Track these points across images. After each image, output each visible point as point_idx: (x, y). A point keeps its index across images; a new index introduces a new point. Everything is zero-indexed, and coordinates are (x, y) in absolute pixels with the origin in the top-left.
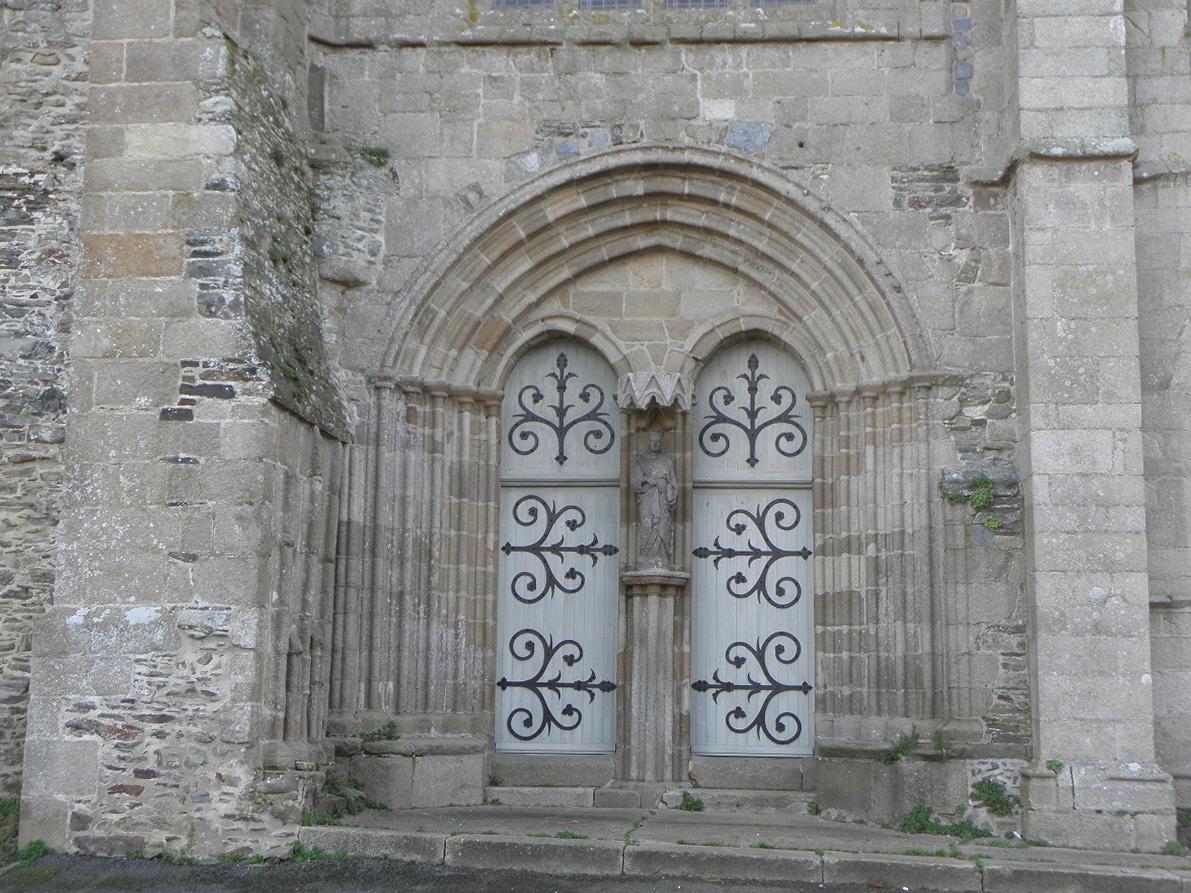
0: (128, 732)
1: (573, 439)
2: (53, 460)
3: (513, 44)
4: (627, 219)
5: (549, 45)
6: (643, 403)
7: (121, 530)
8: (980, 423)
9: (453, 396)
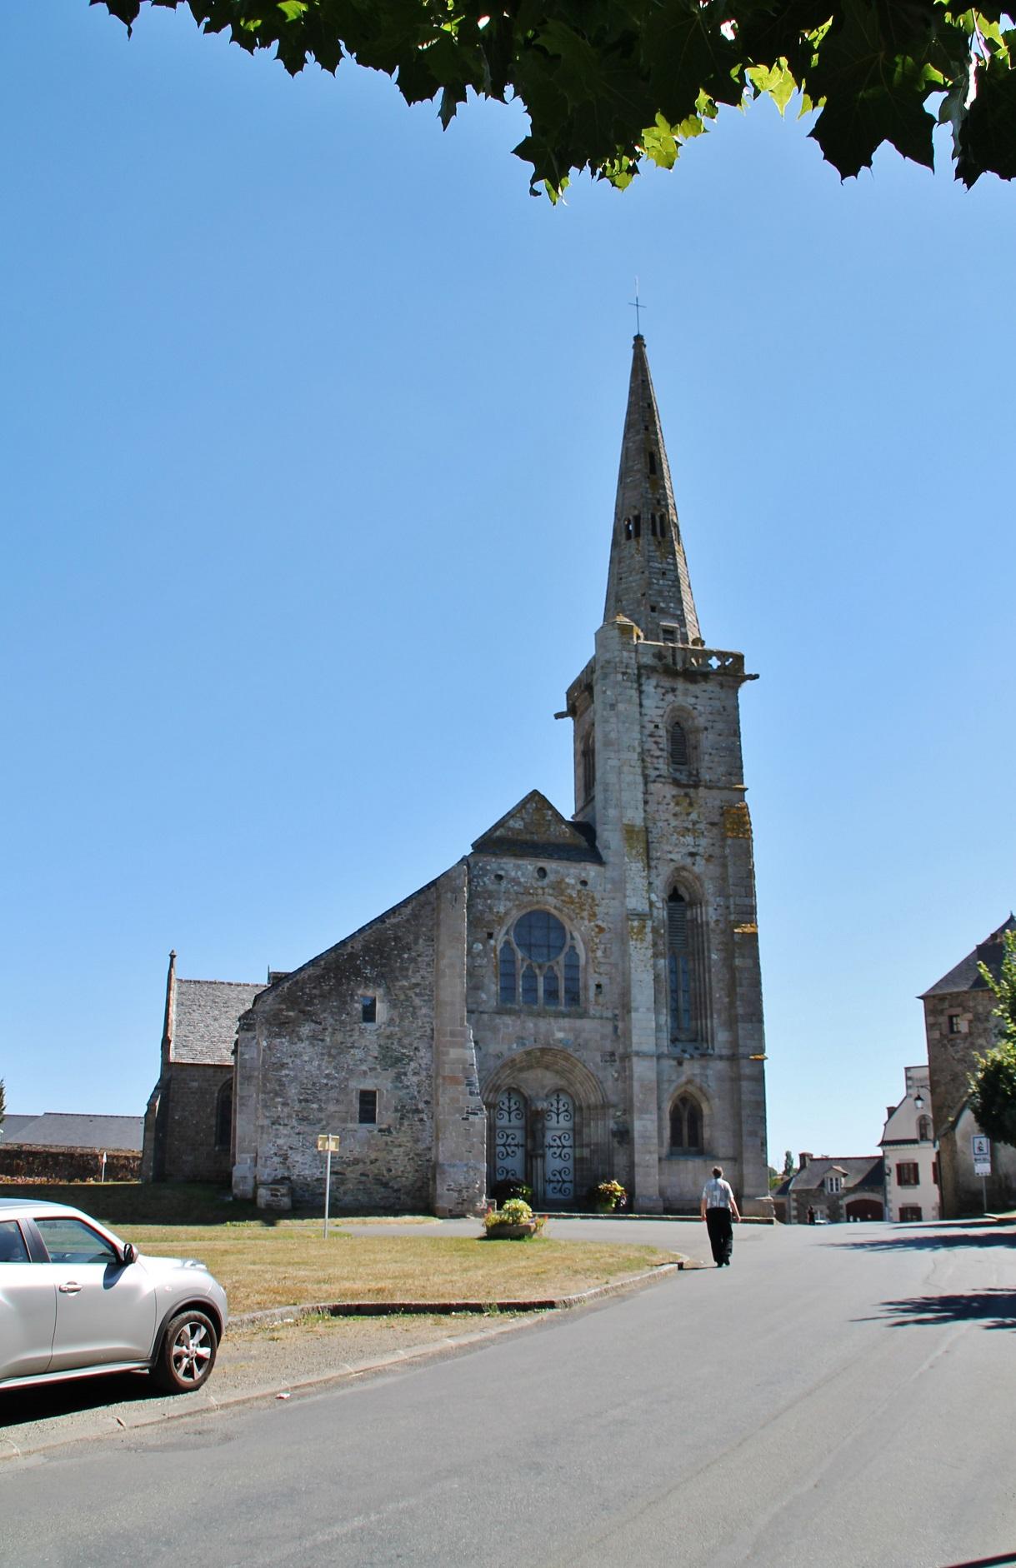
6: (540, 1109)
8: (619, 1116)
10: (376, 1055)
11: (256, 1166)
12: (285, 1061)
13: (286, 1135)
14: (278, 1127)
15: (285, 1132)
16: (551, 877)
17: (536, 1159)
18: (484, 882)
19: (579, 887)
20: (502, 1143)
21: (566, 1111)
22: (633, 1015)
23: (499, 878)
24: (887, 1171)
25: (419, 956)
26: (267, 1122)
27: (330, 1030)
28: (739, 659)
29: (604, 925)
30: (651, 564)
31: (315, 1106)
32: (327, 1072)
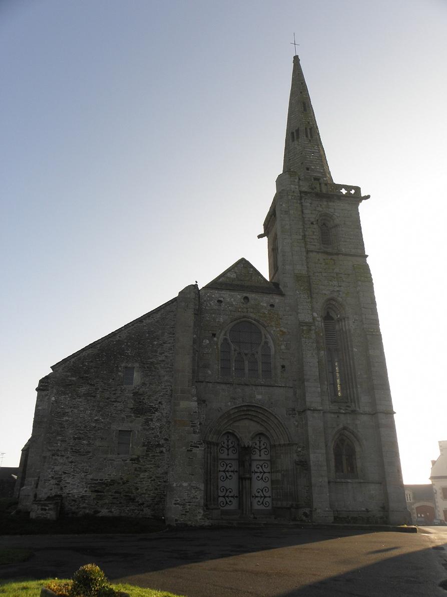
0: (184, 505)
1: (230, 451)
2: (159, 456)
4: (243, 413)
5: (231, 384)
6: (247, 446)
7: (181, 470)
8: (300, 451)
10: (132, 407)
11: (37, 487)
14: (57, 457)
15: (61, 461)
16: (252, 302)
17: (245, 480)
18: (210, 304)
19: (269, 308)
20: (223, 470)
21: (265, 448)
23: (219, 301)
24: (435, 492)
25: (164, 343)
26: (48, 454)
28: (357, 189)
29: (285, 330)
30: (306, 149)
32: (96, 418)
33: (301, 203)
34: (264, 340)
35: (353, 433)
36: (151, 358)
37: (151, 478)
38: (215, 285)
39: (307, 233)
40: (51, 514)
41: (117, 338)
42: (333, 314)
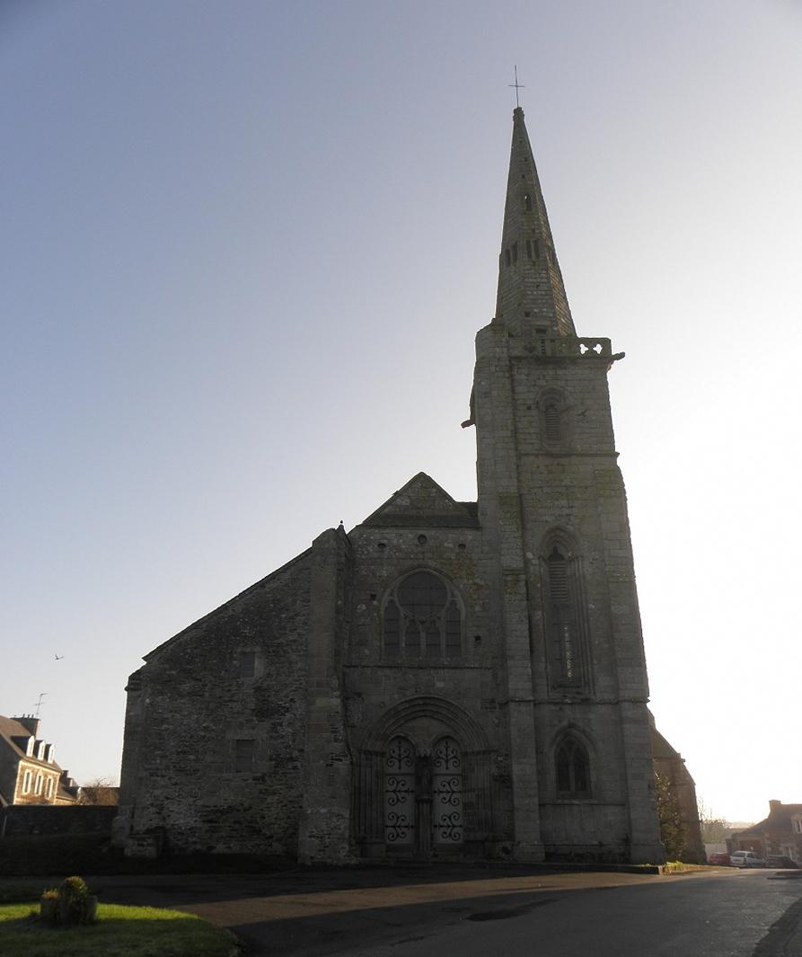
3: (391, 667)
4: (418, 709)
6: (423, 755)
9: (376, 754)
10: (253, 708)
11: (133, 817)
12: (165, 716)
13: (163, 786)
14: (155, 778)
15: (162, 783)
18: (368, 551)
19: (457, 550)
21: (455, 757)
22: (510, 663)
23: (382, 545)
27: (209, 685)
28: (606, 343)
29: (482, 583)
30: (527, 280)
31: (192, 757)
33: (512, 376)
34: (449, 599)
35: (584, 732)
36: (277, 639)
37: (281, 802)
38: (380, 519)
39: (520, 425)
40: (150, 851)
41: (230, 612)
42: (562, 551)
